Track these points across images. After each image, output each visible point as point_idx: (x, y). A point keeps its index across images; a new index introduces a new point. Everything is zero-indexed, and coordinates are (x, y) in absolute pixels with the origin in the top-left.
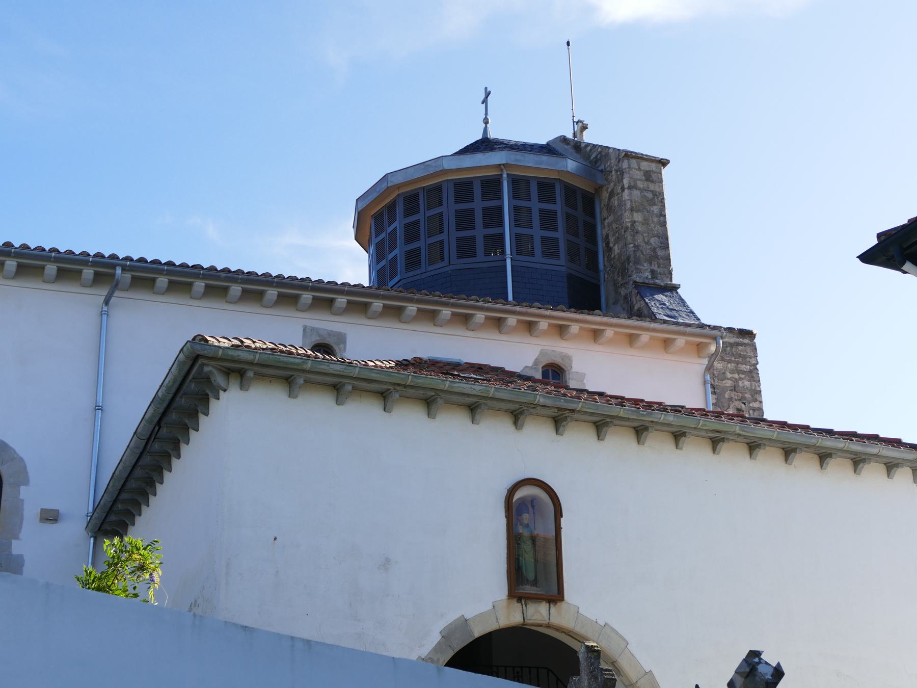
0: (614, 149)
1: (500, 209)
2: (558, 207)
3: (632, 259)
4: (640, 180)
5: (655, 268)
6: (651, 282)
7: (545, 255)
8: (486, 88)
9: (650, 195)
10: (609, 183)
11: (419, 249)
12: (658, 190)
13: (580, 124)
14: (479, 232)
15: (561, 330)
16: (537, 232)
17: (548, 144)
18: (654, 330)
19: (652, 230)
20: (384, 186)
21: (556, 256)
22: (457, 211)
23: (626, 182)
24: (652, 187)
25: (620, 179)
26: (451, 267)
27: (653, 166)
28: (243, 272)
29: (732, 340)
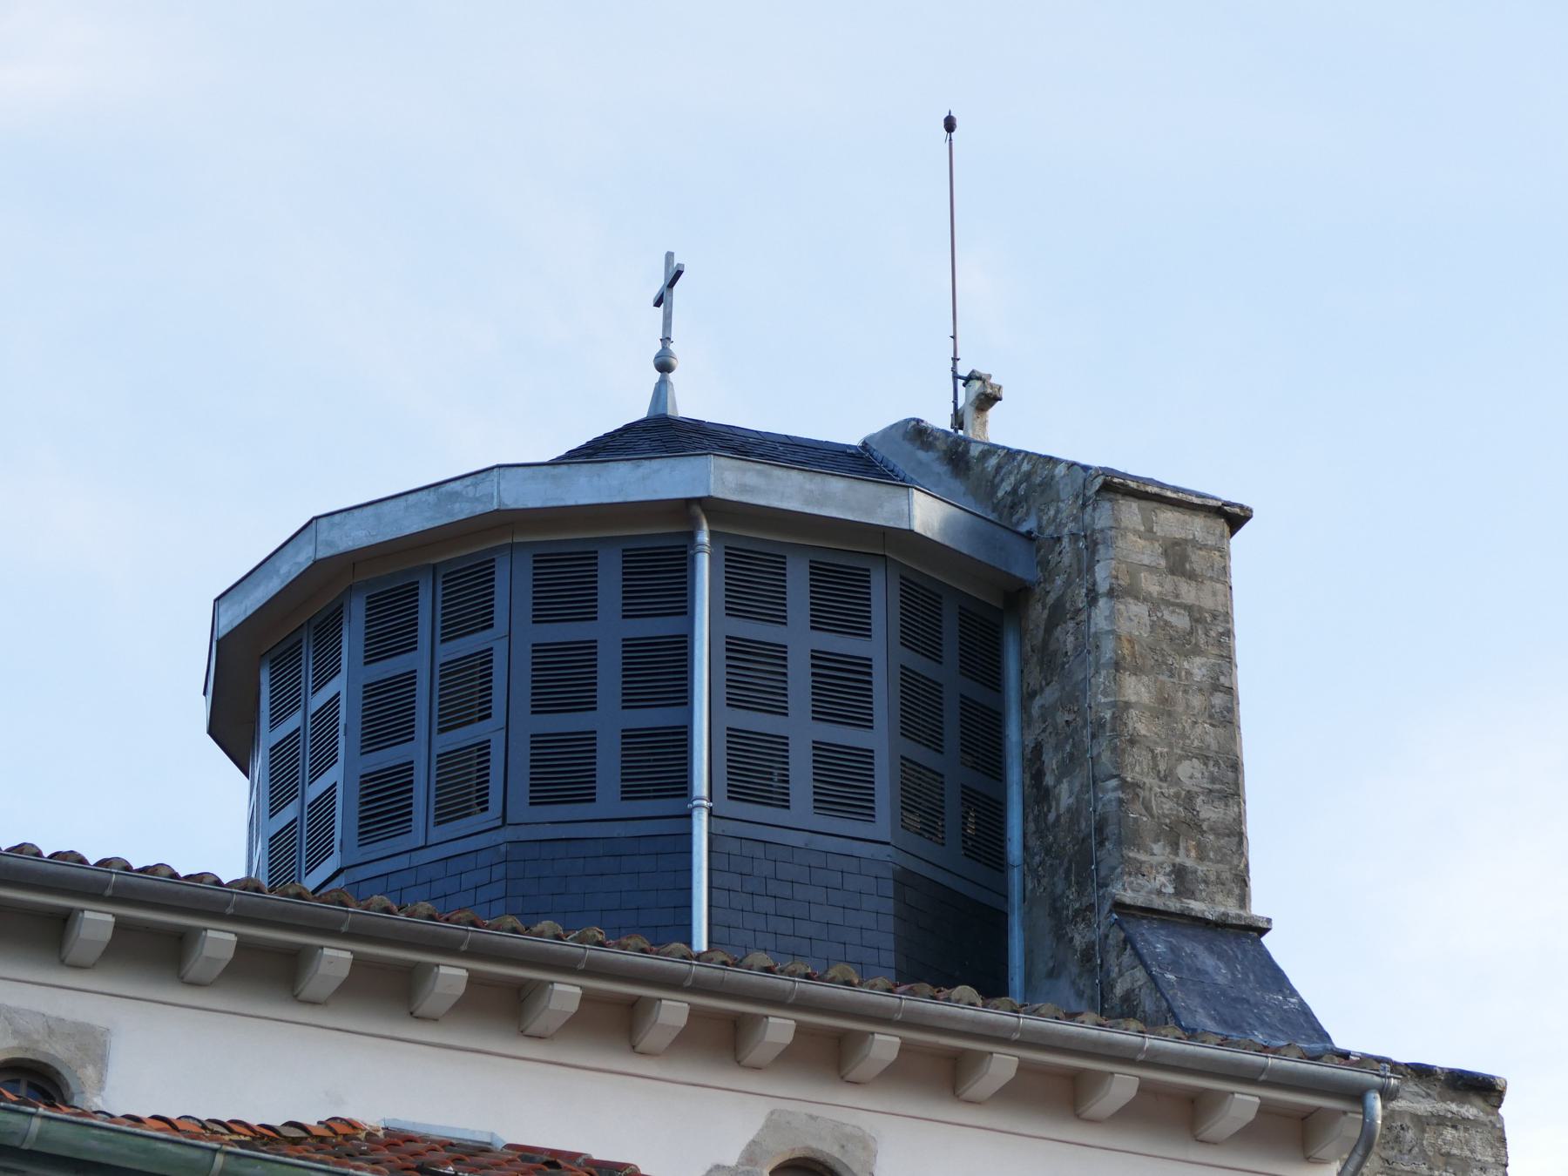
0: (1072, 465)
1: (682, 646)
2: (879, 647)
3: (1111, 829)
4: (1151, 569)
5: (1189, 863)
6: (1174, 905)
7: (823, 803)
8: (669, 256)
9: (1181, 621)
10: (1049, 579)
11: (407, 768)
12: (1208, 603)
13: (976, 385)
14: (609, 720)
15: (829, 1053)
16: (801, 730)
17: (865, 445)
18: (1154, 1061)
19: (1184, 736)
20: (303, 558)
21: (863, 808)
22: (537, 648)
23: (1102, 574)
24: (1188, 592)
25: (1086, 564)
26: (509, 834)
27: (1198, 527)
28: (128, 868)
29: (1424, 1107)
